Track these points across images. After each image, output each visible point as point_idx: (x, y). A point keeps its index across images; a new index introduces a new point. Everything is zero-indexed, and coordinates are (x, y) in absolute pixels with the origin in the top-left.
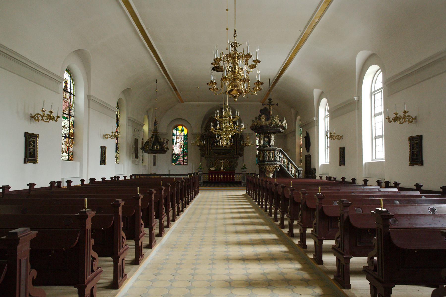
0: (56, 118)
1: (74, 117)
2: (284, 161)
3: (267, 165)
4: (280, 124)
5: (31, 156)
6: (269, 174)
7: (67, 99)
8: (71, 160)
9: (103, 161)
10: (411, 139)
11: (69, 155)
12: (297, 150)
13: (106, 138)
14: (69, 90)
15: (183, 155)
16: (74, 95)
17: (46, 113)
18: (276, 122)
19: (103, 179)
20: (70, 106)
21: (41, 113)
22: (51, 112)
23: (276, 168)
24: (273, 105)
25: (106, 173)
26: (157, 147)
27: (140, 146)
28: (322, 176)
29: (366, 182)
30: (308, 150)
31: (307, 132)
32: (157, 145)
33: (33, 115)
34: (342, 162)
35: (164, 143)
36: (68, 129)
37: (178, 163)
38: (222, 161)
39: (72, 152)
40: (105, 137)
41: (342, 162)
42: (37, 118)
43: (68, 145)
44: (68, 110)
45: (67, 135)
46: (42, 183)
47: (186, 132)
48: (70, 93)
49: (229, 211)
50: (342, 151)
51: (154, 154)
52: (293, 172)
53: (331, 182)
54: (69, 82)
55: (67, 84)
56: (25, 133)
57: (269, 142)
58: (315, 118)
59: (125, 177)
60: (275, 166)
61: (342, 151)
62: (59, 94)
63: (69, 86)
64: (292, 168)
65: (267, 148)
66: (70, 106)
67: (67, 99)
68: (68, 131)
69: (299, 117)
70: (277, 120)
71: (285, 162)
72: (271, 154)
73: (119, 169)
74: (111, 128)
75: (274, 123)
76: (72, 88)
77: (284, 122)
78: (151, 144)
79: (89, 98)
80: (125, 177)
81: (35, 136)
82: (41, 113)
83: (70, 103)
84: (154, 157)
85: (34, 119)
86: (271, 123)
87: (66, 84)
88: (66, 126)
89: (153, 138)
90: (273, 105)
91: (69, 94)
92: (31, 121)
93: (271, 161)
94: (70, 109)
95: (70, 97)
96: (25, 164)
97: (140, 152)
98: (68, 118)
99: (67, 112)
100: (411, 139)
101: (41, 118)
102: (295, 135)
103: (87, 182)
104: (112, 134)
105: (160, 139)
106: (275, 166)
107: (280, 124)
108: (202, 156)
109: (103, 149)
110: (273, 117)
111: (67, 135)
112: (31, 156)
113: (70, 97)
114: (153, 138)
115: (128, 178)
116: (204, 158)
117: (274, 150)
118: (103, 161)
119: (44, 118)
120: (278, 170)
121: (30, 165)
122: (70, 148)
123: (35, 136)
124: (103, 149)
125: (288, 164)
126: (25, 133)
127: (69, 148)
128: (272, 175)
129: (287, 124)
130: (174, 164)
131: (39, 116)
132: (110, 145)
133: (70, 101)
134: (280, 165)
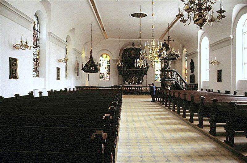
0: (30, 47)
1: (39, 47)
2: (178, 79)
3: (167, 81)
4: (176, 53)
5: (13, 74)
6: (168, 87)
7: (35, 35)
8: (38, 77)
9: (58, 78)
10: (218, 71)
11: (37, 74)
12: (184, 71)
13: (60, 62)
14: (36, 29)
15: (107, 74)
16: (39, 32)
17: (24, 43)
18: (173, 52)
19: (31, 94)
20: (37, 39)
21: (20, 44)
22: (26, 43)
23: (173, 83)
24: (171, 40)
25: (59, 86)
26: (93, 69)
27: (80, 67)
28: (203, 89)
29: (235, 93)
30: (192, 72)
31: (192, 59)
32: (91, 67)
33: (15, 45)
34: (219, 80)
35: (97, 65)
36: (36, 55)
37: (103, 79)
38: (133, 78)
39: (38, 71)
40: (59, 61)
41: (219, 80)
42: (17, 47)
43: (36, 66)
44: (36, 42)
45: (36, 60)
46: (24, 93)
47: (108, 59)
48: (37, 31)
49: (153, 110)
50: (220, 72)
51: (88, 73)
52: (183, 86)
53: (211, 93)
54: (36, 23)
55: (35, 24)
56: (10, 58)
57: (168, 66)
58: (198, 51)
59: (70, 89)
60: (172, 82)
61: (220, 72)
62: (31, 30)
63: (36, 26)
64: (183, 83)
65: (167, 70)
66: (37, 39)
67: (35, 35)
68: (36, 57)
69: (185, 50)
70: (173, 51)
71: (178, 79)
72: (170, 74)
73: (68, 83)
74: (63, 56)
75: (172, 53)
76: (38, 27)
77: (178, 52)
78: (89, 66)
79: (50, 34)
80: (70, 89)
81: (16, 60)
82: (20, 44)
83: (37, 37)
84: (88, 75)
85: (15, 47)
86: (170, 52)
87: (35, 24)
88: (35, 54)
89: (90, 62)
90: (171, 40)
91: (36, 32)
92: (13, 49)
93: (170, 78)
94: (37, 42)
95: (37, 33)
96: (10, 80)
97: (82, 72)
98: (36, 48)
99: (35, 44)
100: (218, 71)
101: (20, 47)
102: (182, 61)
103: (68, 90)
104: (64, 59)
105: (95, 63)
106: (172, 82)
107: (176, 53)
108: (119, 75)
109: (58, 69)
110: (172, 49)
111: (36, 60)
112: (13, 74)
113: (37, 33)
114: (90, 62)
115: (45, 94)
116: (121, 76)
117: (172, 71)
118: (58, 78)
119: (22, 47)
120: (174, 84)
121: (13, 80)
122: (37, 68)
123: (16, 60)
124: (58, 69)
125: (180, 81)
126: (10, 58)
127: (37, 69)
128: (169, 88)
129: (180, 53)
130: (101, 80)
131: (19, 45)
132: (62, 66)
133: (37, 36)
134: (175, 81)
